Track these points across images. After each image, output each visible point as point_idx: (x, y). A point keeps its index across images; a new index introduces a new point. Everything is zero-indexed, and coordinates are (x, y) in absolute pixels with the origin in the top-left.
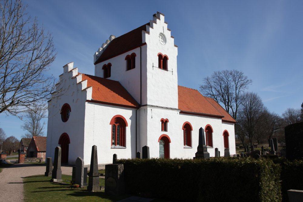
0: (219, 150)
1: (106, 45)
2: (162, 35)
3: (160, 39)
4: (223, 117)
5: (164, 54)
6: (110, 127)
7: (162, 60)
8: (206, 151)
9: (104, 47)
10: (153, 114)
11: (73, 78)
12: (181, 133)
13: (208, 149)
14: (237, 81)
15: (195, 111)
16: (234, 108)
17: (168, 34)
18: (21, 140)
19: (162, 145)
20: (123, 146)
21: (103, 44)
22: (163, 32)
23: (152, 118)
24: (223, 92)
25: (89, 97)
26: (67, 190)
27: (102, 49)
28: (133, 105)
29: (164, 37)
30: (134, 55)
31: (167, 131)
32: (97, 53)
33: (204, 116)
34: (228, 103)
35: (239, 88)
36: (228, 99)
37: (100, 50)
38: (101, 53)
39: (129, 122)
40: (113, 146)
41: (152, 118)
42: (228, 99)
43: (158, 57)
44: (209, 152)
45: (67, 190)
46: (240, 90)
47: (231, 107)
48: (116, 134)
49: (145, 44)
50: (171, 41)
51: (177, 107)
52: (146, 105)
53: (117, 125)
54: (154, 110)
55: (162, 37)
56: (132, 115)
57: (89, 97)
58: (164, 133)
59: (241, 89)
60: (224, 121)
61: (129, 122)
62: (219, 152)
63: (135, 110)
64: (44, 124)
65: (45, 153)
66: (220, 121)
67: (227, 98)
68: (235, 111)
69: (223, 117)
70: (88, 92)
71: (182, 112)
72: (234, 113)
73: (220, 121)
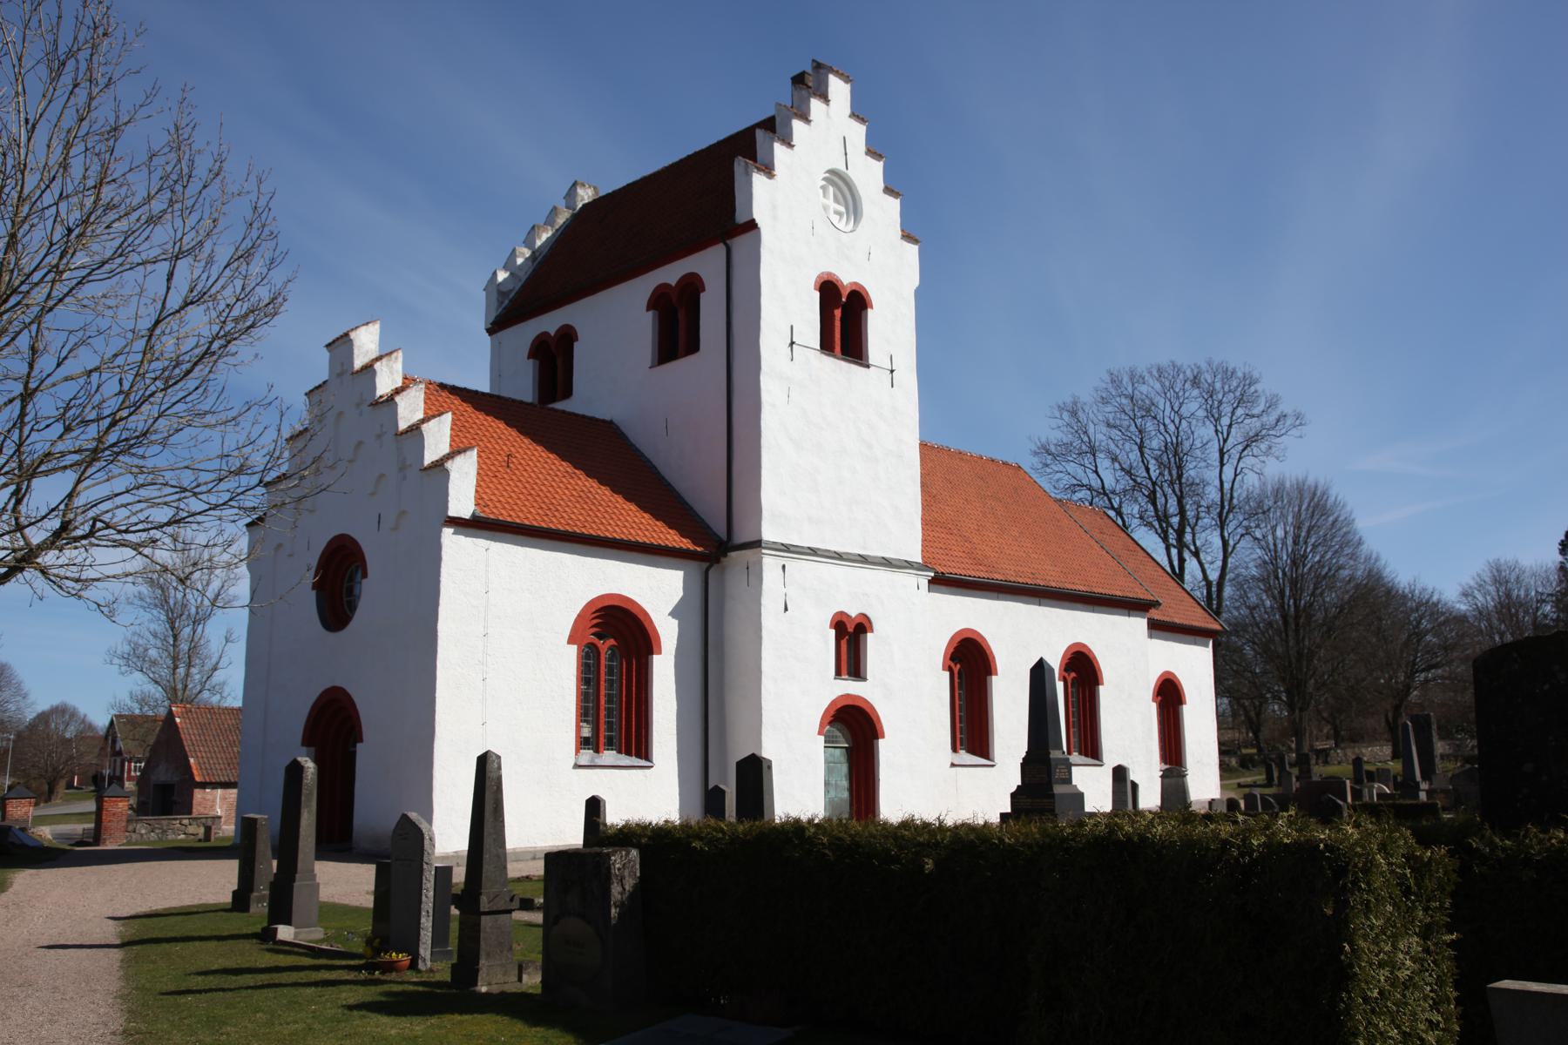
0: (1133, 776)
1: (550, 234)
2: (839, 182)
3: (825, 201)
4: (1155, 604)
5: (847, 277)
7: (838, 313)
8: (1068, 780)
9: (539, 243)
11: (376, 403)
14: (1225, 421)
16: (1209, 559)
17: (868, 175)
18: (107, 723)
20: (639, 756)
24: (1154, 475)
25: (462, 501)
27: (527, 253)
28: (686, 544)
30: (692, 287)
31: (865, 679)
32: (502, 276)
34: (1180, 533)
35: (1235, 453)
36: (1182, 512)
37: (520, 261)
39: (668, 631)
41: (786, 609)
42: (1182, 512)
44: (1081, 788)
46: (1241, 465)
47: (1196, 554)
49: (752, 226)
50: (884, 212)
51: (917, 558)
52: (757, 544)
54: (797, 566)
56: (681, 594)
57: (462, 501)
58: (851, 687)
59: (1248, 461)
60: (1159, 628)
61: (668, 631)
62: (1135, 786)
63: (696, 567)
65: (235, 791)
66: (1139, 624)
67: (1173, 507)
68: (1214, 576)
69: (1155, 604)
70: (454, 476)
71: (941, 582)
72: (1209, 584)
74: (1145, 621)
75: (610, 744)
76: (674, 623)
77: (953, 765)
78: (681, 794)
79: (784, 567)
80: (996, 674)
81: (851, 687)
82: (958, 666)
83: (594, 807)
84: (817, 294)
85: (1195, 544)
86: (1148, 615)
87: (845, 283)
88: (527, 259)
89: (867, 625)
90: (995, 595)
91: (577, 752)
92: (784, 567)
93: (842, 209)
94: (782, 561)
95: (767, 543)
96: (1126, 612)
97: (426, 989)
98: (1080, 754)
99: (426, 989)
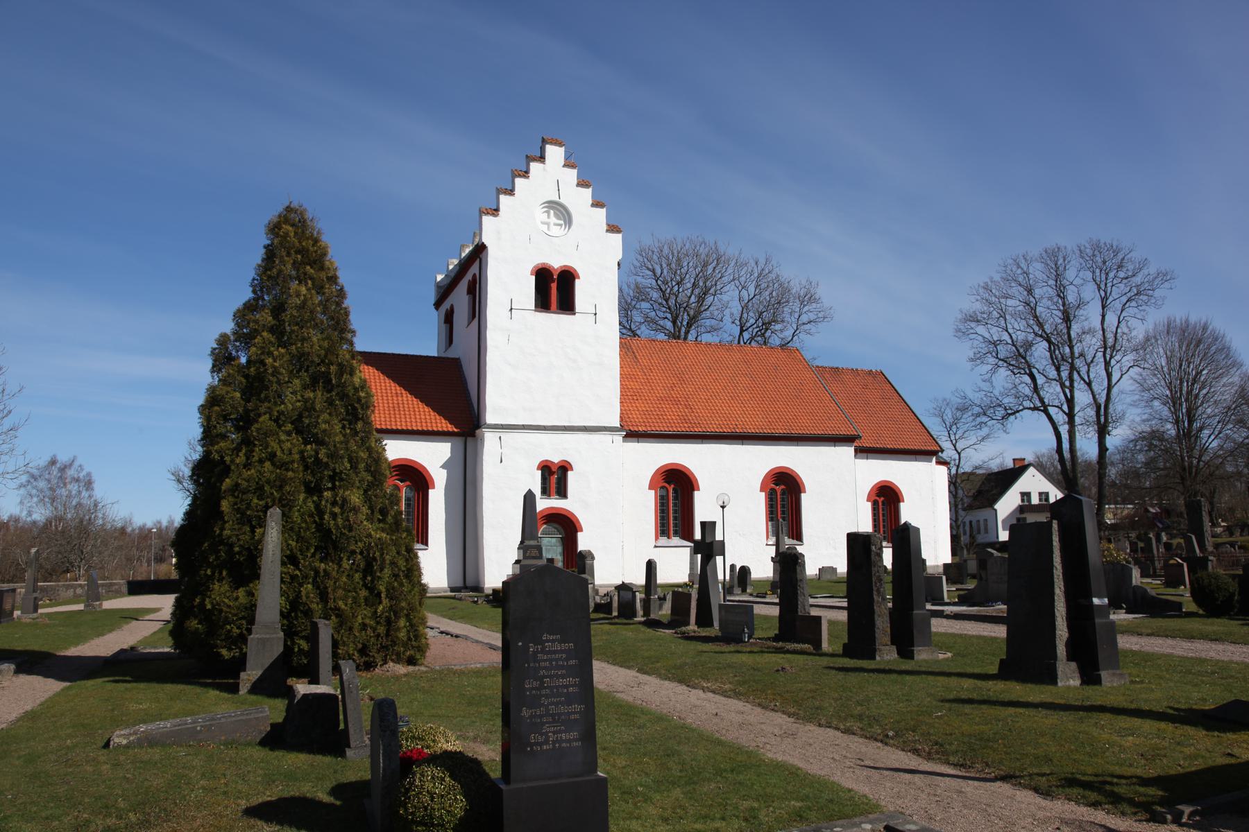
1: (471, 248)
4: (858, 437)
5: (556, 263)
6: (761, 499)
9: (463, 255)
10: (504, 451)
12: (758, 504)
13: (884, 549)
15: (713, 428)
19: (554, 540)
20: (422, 543)
21: (462, 247)
22: (557, 199)
23: (501, 462)
26: (948, 776)
27: (456, 262)
28: (451, 428)
29: (564, 212)
33: (762, 442)
38: (453, 275)
39: (439, 477)
40: (663, 541)
41: (501, 462)
43: (532, 280)
45: (948, 776)
46: (1124, 314)
48: (881, 518)
53: (779, 489)
54: (508, 436)
55: (558, 210)
56: (449, 455)
59: (1130, 311)
60: (863, 452)
61: (439, 477)
64: (723, 507)
66: (849, 451)
68: (1102, 400)
69: (858, 437)
71: (633, 435)
73: (848, 451)
74: (852, 449)
75: (676, 534)
76: (444, 472)
77: (656, 547)
78: (447, 564)
79: (500, 438)
80: (698, 489)
81: (555, 503)
82: (672, 486)
83: (651, 567)
84: (533, 278)
85: (1089, 376)
86: (855, 444)
87: (556, 267)
88: (456, 265)
89: (568, 466)
90: (700, 441)
91: (657, 538)
92: (500, 438)
93: (562, 222)
94: (499, 435)
95: (489, 425)
96: (833, 443)
97: (1176, 713)
98: (789, 538)
99: (1176, 713)
